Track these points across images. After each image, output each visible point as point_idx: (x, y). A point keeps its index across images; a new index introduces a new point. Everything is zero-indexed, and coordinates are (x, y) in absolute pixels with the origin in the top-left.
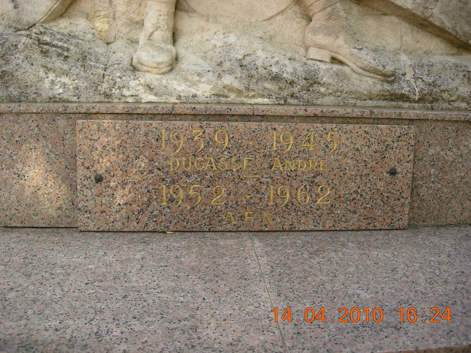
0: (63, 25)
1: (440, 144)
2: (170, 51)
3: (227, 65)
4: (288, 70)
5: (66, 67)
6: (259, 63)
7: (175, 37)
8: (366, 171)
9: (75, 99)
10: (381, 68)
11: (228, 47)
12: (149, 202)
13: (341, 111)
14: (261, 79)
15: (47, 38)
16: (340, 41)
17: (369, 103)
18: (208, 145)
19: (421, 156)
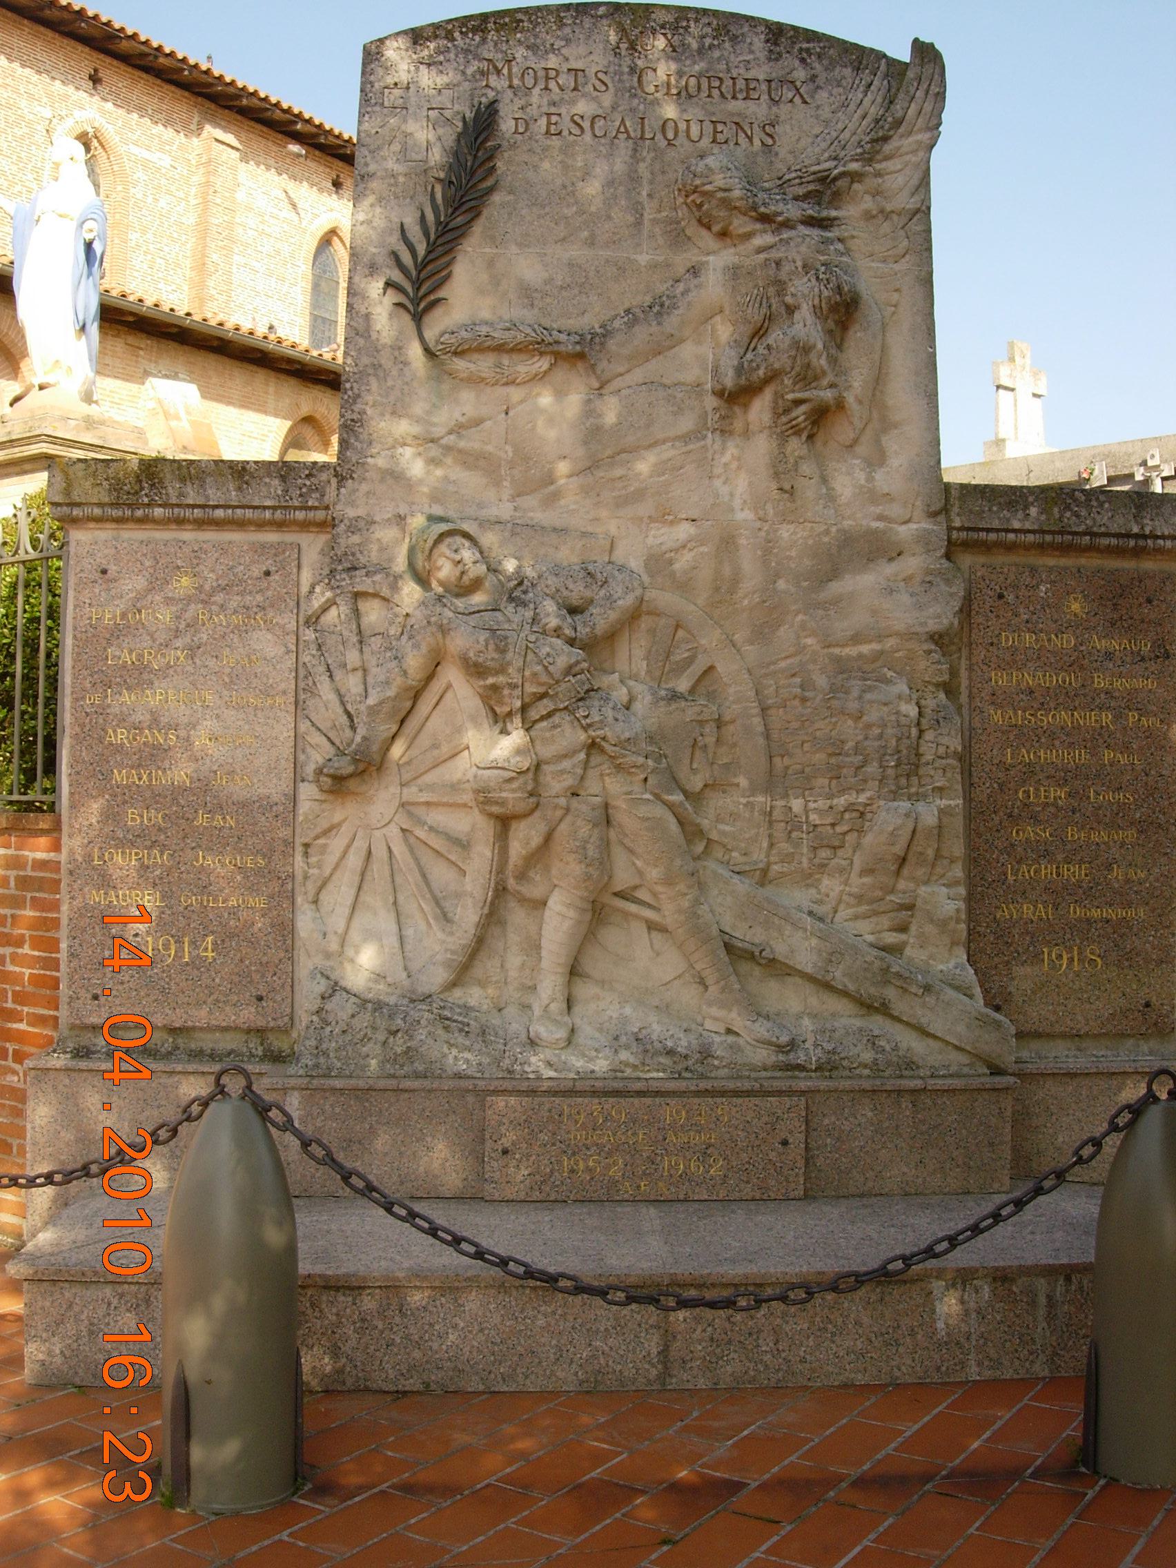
0: (457, 993)
1: (835, 1113)
2: (566, 1024)
3: (623, 1039)
4: (683, 1043)
5: (467, 1043)
6: (654, 1037)
7: (570, 1003)
8: (757, 1143)
9: (479, 1075)
10: (774, 1039)
11: (624, 1020)
12: (552, 1171)
13: (731, 1085)
14: (657, 1053)
15: (447, 1013)
16: (734, 1015)
17: (764, 1074)
18: (605, 1120)
19: (815, 1126)
